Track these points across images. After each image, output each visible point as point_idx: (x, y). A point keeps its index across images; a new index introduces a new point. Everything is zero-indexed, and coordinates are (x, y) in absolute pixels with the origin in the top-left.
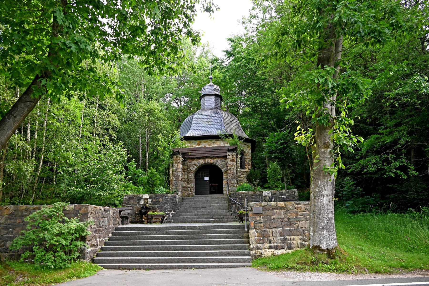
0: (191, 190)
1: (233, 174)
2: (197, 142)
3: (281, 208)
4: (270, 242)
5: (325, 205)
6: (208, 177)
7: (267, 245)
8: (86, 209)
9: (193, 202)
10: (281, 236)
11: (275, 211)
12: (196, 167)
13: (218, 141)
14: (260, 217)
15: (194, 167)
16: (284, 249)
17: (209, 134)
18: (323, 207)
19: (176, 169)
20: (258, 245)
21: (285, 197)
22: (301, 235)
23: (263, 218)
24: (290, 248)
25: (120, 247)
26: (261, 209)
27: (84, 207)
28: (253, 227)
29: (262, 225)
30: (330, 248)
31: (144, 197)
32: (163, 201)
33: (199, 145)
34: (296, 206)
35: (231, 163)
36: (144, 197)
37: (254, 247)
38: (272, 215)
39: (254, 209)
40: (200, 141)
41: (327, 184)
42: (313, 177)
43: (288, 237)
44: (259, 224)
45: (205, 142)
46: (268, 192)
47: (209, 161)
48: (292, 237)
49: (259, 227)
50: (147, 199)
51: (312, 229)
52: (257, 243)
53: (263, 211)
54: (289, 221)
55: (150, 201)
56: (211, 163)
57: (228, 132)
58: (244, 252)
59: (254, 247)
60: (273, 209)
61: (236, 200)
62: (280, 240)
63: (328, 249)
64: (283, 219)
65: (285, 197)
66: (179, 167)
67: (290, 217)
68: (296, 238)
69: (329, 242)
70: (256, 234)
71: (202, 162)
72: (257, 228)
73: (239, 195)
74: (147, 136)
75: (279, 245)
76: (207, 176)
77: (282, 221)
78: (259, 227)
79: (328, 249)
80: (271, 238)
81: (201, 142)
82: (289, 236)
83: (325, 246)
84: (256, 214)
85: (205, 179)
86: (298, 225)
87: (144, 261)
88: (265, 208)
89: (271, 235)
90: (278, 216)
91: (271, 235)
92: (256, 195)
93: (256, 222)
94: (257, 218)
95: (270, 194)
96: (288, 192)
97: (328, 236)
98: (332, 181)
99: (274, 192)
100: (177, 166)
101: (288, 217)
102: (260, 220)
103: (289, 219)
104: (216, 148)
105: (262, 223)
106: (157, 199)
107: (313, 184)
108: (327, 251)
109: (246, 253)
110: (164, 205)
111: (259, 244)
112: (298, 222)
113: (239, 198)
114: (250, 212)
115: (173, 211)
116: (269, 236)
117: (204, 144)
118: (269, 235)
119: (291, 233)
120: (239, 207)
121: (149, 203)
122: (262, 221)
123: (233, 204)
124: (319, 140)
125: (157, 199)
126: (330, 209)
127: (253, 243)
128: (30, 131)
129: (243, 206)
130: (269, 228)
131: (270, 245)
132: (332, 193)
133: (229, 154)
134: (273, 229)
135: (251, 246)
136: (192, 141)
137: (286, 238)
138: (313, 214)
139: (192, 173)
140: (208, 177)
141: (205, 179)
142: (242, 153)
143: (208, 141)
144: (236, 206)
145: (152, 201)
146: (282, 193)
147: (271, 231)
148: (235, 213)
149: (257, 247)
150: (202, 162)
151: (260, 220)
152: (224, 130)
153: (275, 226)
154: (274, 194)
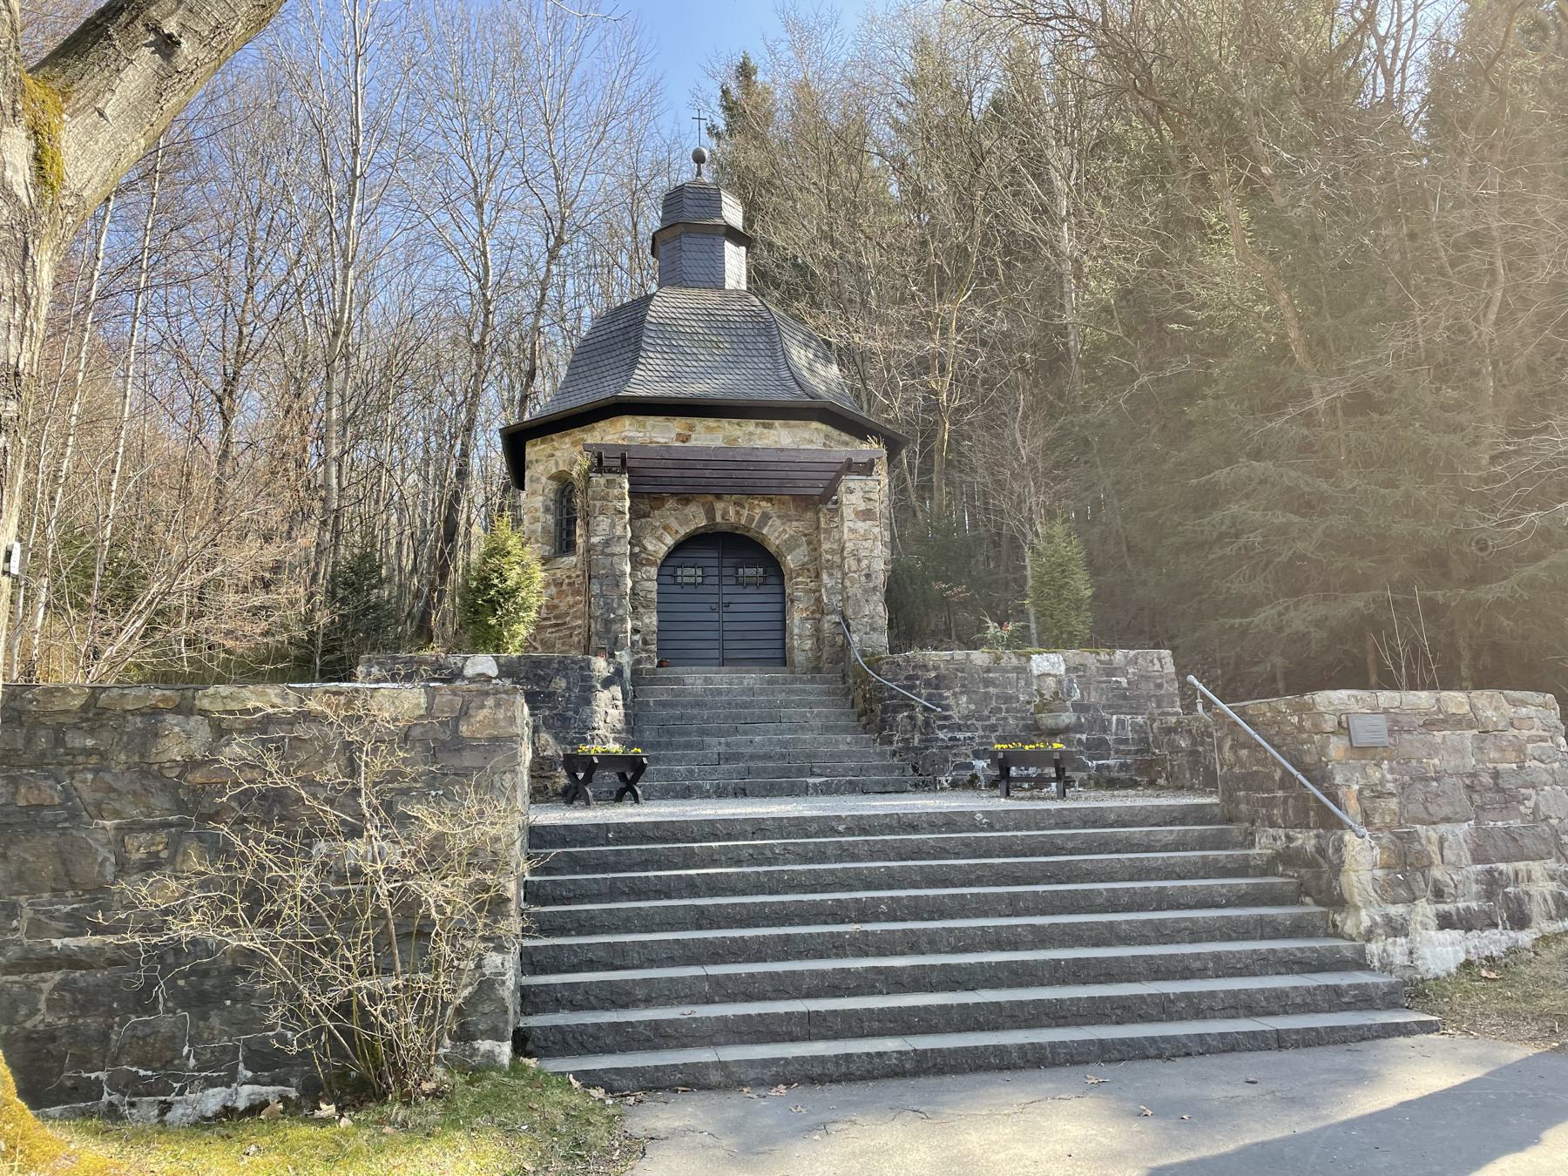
0: (645, 642)
1: (868, 576)
3: (1458, 722)
4: (1439, 894)
8: (501, 715)
10: (1476, 861)
11: (1438, 736)
12: (670, 541)
14: (1378, 765)
15: (660, 539)
16: (1496, 926)
19: (607, 543)
21: (1124, 681)
23: (1392, 771)
24: (1520, 920)
25: (643, 944)
26: (1381, 722)
27: (490, 702)
31: (469, 671)
32: (568, 689)
34: (1510, 711)
35: (861, 526)
36: (469, 671)
37: (1375, 924)
38: (1430, 756)
39: (1356, 724)
40: (690, 420)
43: (1502, 866)
44: (1382, 803)
46: (1053, 657)
48: (1521, 865)
53: (1391, 732)
54: (1499, 790)
58: (1337, 950)
59: (1375, 924)
60: (1430, 725)
61: (910, 688)
65: (1124, 681)
66: (619, 531)
67: (1500, 766)
68: (1537, 868)
70: (1377, 851)
72: (1377, 820)
73: (925, 667)
74: (43, 493)
75: (1474, 905)
80: (1437, 873)
82: (1506, 860)
87: (640, 993)
88: (1396, 722)
89: (1437, 859)
90: (1452, 763)
91: (1437, 859)
92: (1005, 671)
95: (1063, 668)
96: (1134, 661)
99: (1078, 660)
100: (613, 525)
105: (1391, 794)
106: (544, 679)
109: (1348, 954)
110: (577, 712)
111: (1394, 903)
113: (928, 684)
114: (1333, 739)
116: (1431, 864)
117: (709, 436)
118: (1430, 857)
120: (927, 723)
122: (1390, 786)
123: (896, 710)
125: (544, 679)
129: (946, 718)
130: (1423, 822)
133: (851, 484)
134: (1443, 828)
139: (651, 563)
143: (725, 422)
144: (911, 718)
146: (1110, 662)
147: (1434, 836)
148: (908, 749)
149: (1389, 920)
151: (1382, 782)
152: (792, 384)
153: (1447, 810)
154: (1076, 669)
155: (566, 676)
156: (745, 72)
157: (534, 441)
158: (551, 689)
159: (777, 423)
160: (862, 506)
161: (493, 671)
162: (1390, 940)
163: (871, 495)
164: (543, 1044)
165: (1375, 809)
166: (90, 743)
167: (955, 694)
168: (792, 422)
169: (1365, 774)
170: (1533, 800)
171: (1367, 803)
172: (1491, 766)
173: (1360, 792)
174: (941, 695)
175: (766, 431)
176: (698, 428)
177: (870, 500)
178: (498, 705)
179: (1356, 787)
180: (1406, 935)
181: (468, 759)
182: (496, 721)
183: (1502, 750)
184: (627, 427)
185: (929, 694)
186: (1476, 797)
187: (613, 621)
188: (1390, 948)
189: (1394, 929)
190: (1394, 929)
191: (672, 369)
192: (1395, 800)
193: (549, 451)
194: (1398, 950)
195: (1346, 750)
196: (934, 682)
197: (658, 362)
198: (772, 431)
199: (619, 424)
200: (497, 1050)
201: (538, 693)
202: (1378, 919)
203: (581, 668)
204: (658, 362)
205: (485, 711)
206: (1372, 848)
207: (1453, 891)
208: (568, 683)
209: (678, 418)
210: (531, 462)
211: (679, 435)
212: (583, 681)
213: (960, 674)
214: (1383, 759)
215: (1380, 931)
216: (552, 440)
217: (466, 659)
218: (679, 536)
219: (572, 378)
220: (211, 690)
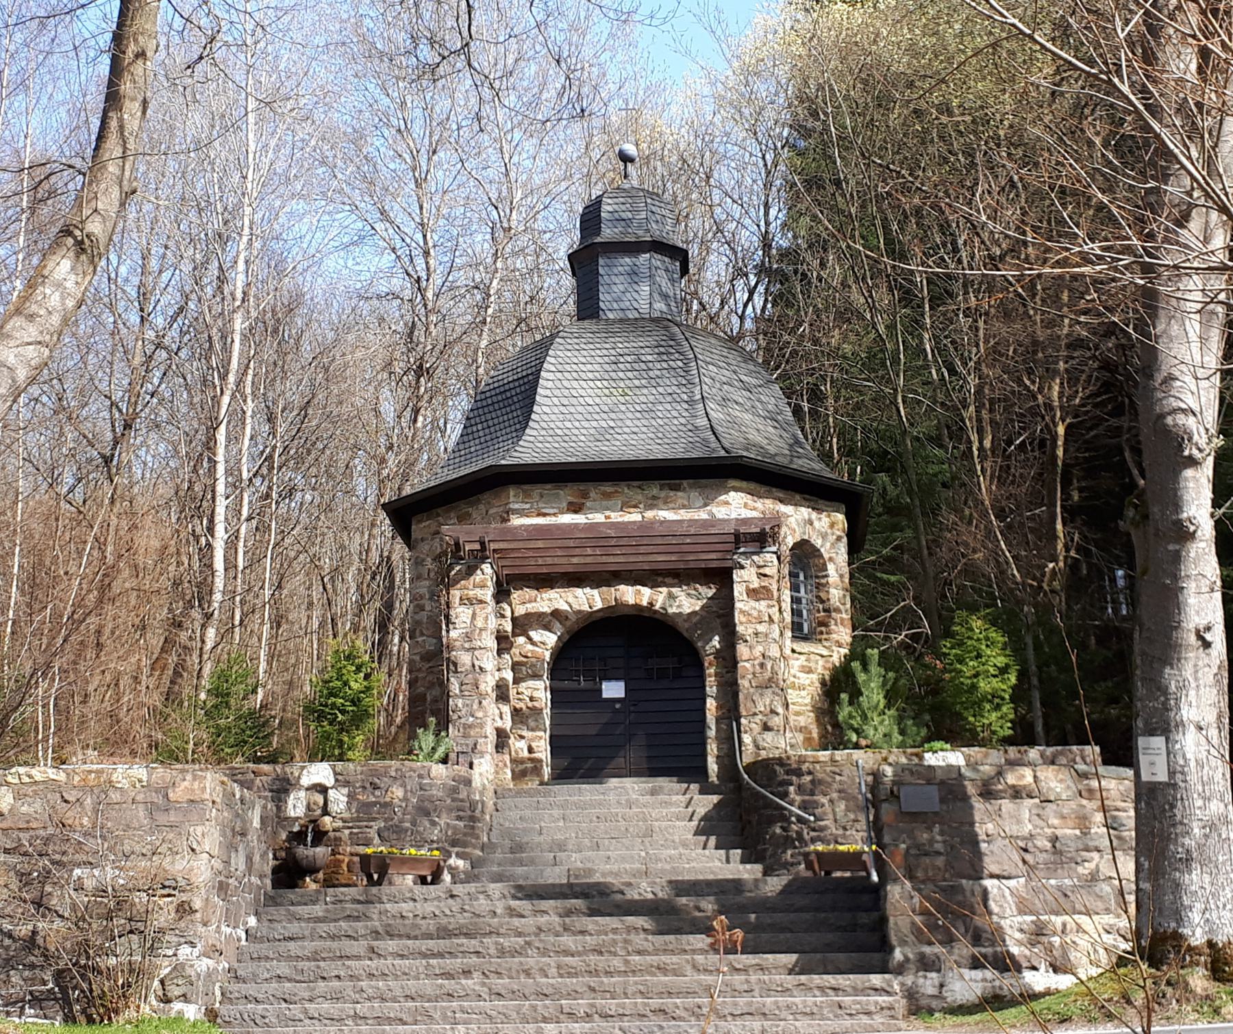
2: (567, 494)
5: (1193, 764)
6: (621, 684)
7: (964, 949)
10: (1021, 912)
13: (677, 488)
14: (930, 829)
18: (1183, 773)
19: (468, 637)
20: (927, 950)
22: (1108, 911)
23: (942, 833)
26: (934, 791)
29: (940, 861)
30: (1220, 940)
32: (405, 799)
36: (306, 781)
37: (907, 960)
41: (1196, 679)
42: (1143, 654)
44: (927, 860)
47: (632, 595)
49: (926, 871)
50: (322, 789)
51: (1146, 864)
52: (921, 942)
53: (943, 800)
55: (339, 800)
59: (907, 960)
62: (1021, 930)
63: (1211, 944)
66: (479, 623)
67: (1059, 832)
72: (920, 874)
76: (617, 679)
77: (1026, 850)
78: (926, 871)
79: (1211, 944)
81: (585, 495)
84: (914, 816)
85: (606, 694)
86: (1092, 865)
93: (913, 852)
94: (917, 833)
102: (932, 841)
105: (938, 853)
107: (1143, 679)
112: (1095, 855)
113: (800, 789)
115: (458, 855)
119: (1063, 903)
121: (333, 808)
122: (939, 847)
124: (1156, 510)
126: (1211, 780)
127: (903, 943)
128: (1062, 506)
132: (1219, 717)
135: (898, 955)
136: (537, 490)
138: (1147, 804)
140: (621, 684)
141: (606, 694)
145: (351, 797)
155: (404, 785)
157: (419, 517)
158: (388, 799)
159: (685, 483)
160: (755, 583)
161: (329, 781)
163: (767, 571)
164: (227, 1019)
167: (831, 801)
168: (703, 481)
169: (911, 835)
170: (1095, 863)
172: (1049, 831)
174: (817, 805)
175: (672, 493)
176: (592, 494)
177: (765, 575)
179: (903, 846)
180: (939, 971)
182: (193, 790)
184: (512, 499)
185: (803, 801)
186: (1028, 857)
189: (925, 964)
190: (925, 964)
191: (569, 425)
192: (942, 858)
193: (433, 528)
194: (928, 982)
198: (680, 494)
199: (503, 495)
200: (185, 1009)
201: (375, 804)
202: (911, 956)
205: (186, 783)
207: (990, 936)
208: (406, 792)
209: (570, 484)
210: (416, 540)
211: (570, 503)
213: (838, 778)
215: (911, 966)
216: (438, 515)
217: (303, 768)
218: (568, 623)
220: (13, 770)
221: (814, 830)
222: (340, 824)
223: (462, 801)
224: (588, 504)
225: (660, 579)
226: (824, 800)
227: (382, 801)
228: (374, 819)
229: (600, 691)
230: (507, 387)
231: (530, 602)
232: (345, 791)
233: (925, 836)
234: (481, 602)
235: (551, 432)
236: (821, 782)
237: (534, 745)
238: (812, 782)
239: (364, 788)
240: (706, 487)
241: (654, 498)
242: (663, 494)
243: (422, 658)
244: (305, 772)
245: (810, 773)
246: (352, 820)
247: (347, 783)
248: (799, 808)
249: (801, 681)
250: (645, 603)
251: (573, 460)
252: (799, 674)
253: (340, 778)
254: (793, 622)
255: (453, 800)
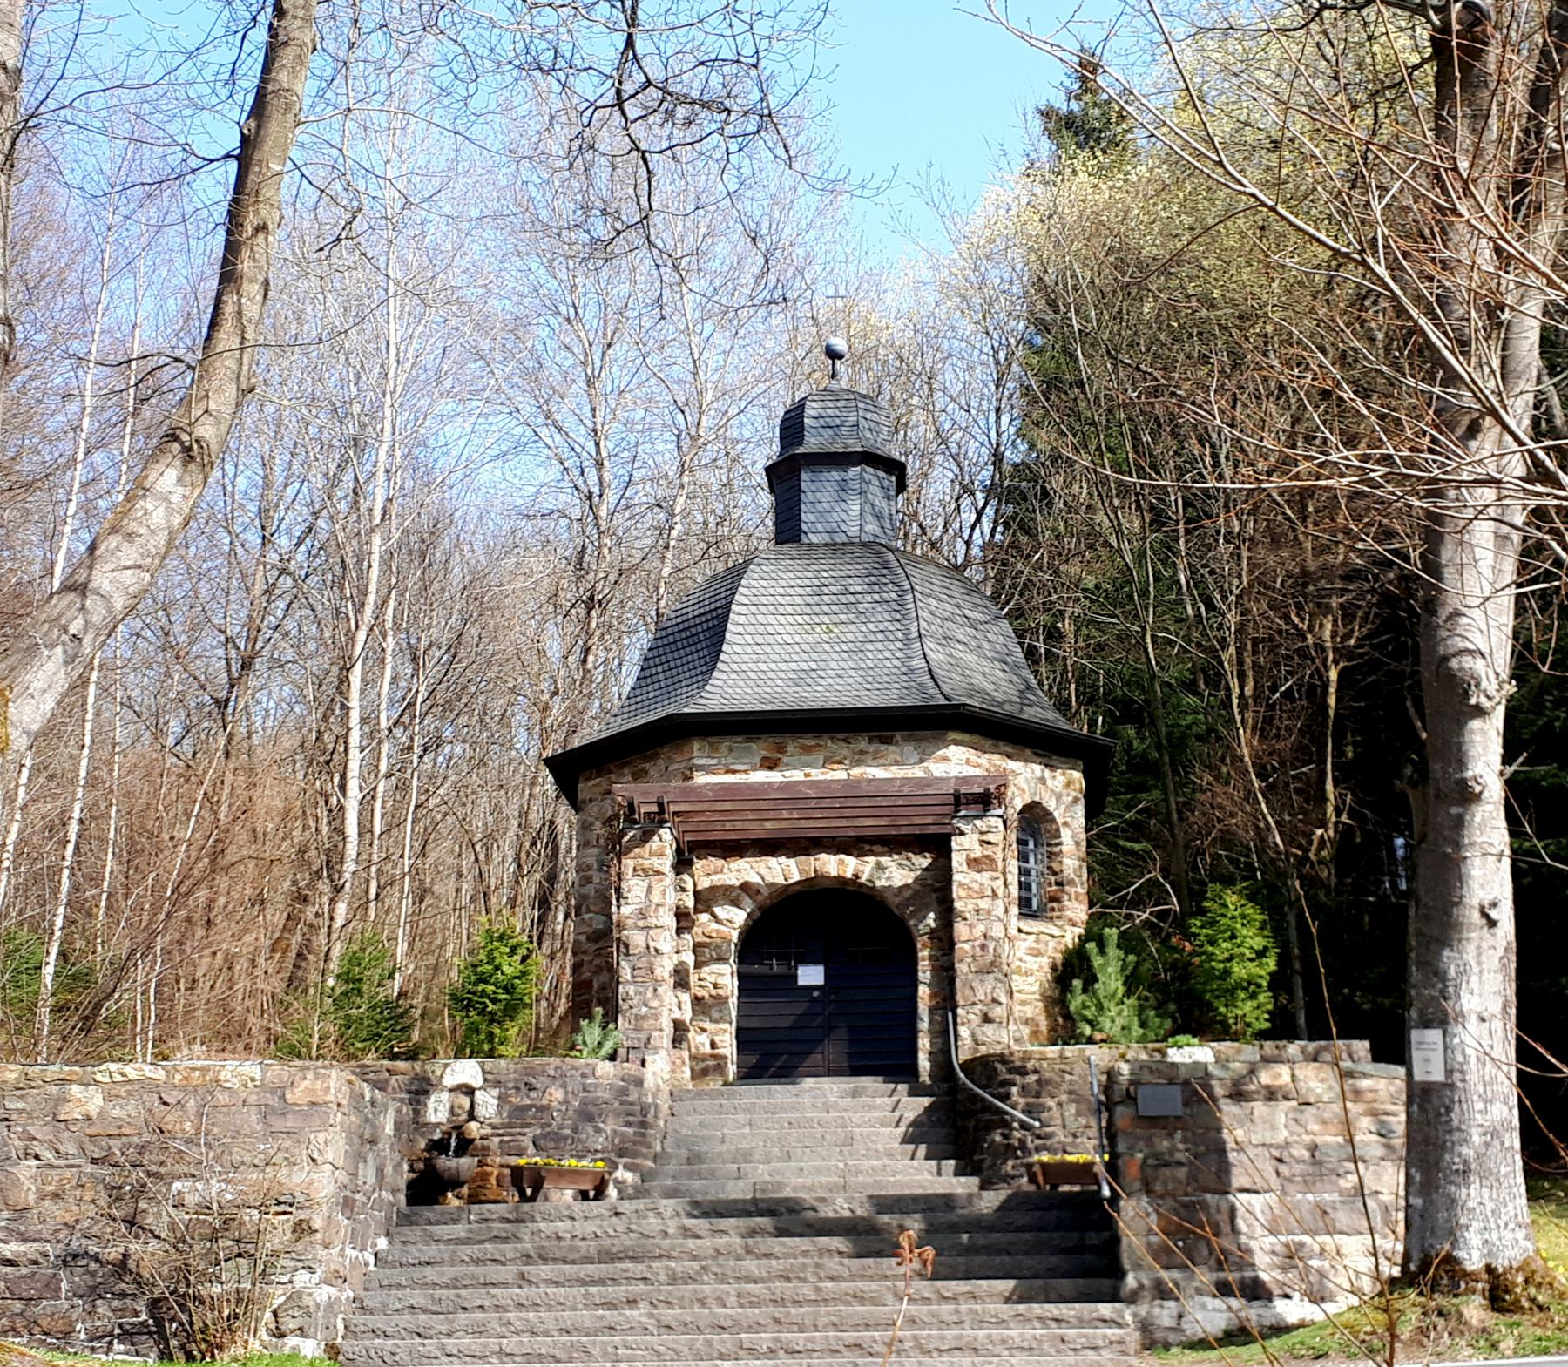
2: (760, 749)
9: (741, 1118)
13: (887, 741)
14: (1170, 1135)
17: (834, 701)
19: (642, 914)
23: (1184, 1140)
28: (1137, 1185)
29: (1182, 1173)
30: (1500, 1264)
32: (566, 1102)
33: (770, 764)
37: (1141, 1287)
41: (1479, 963)
42: (1419, 934)
44: (1167, 1172)
45: (807, 750)
47: (834, 865)
49: (1165, 1183)
53: (1186, 1103)
55: (487, 1103)
56: (841, 880)
57: (946, 689)
59: (1141, 1287)
63: (1490, 1269)
64: (1287, 1145)
66: (656, 897)
67: (1319, 1140)
69: (1495, 1235)
71: (781, 871)
72: (1158, 1188)
76: (815, 962)
77: (1280, 1160)
78: (1165, 1183)
81: (781, 749)
83: (1476, 1254)
84: (1153, 1121)
93: (1150, 1161)
97: (1490, 1206)
98: (1501, 952)
101: (1307, 1138)
103: (1314, 1148)
104: (895, 790)
105: (1180, 1164)
108: (1486, 1277)
113: (1024, 1090)
115: (627, 1167)
121: (480, 1112)
122: (1179, 1156)
127: (1137, 1267)
131: (1221, 1275)
132: (1505, 1007)
135: (1131, 1281)
136: (725, 744)
137: (1302, 1245)
142: (1035, 821)
150: (781, 871)
155: (564, 1086)
156: (1087, 69)
157: (587, 774)
158: (545, 1102)
159: (898, 736)
160: (977, 852)
161: (476, 1080)
162: (1157, 1302)
163: (990, 837)
165: (1156, 1178)
166: (20, 1106)
167: (1060, 1104)
171: (1149, 1171)
173: (1145, 1160)
175: (883, 747)
176: (790, 749)
177: (989, 843)
178: (316, 1078)
179: (1140, 1156)
181: (291, 1122)
183: (1324, 1122)
184: (696, 753)
185: (1028, 1104)
187: (644, 1018)
188: (1157, 1311)
191: (764, 667)
193: (605, 787)
194: (1165, 1312)
195: (1133, 1119)
196: (1035, 1087)
197: (746, 658)
198: (891, 748)
201: (530, 1107)
202: (1146, 1282)
203: (584, 1076)
204: (746, 658)
206: (1148, 1215)
208: (566, 1093)
212: (585, 1090)
213: (1068, 1077)
214: (1176, 1129)
217: (446, 1066)
218: (760, 898)
219: (643, 682)
220: (104, 1067)
221: (1039, 1137)
222: (488, 1130)
223: (631, 1104)
224: (785, 759)
225: (867, 847)
226: (1051, 1103)
227: (538, 1103)
228: (528, 1125)
229: (796, 976)
230: (692, 623)
231: (716, 873)
232: (496, 1092)
233: (1165, 1143)
234: (658, 873)
235: (743, 675)
236: (1048, 1082)
237: (717, 1039)
238: (1039, 1082)
239: (517, 1089)
240: (922, 739)
241: (862, 752)
242: (872, 748)
243: (588, 939)
244: (448, 1070)
245: (1036, 1071)
246: (504, 1126)
247: (497, 1084)
248: (1023, 1112)
249: (1028, 966)
250: (849, 875)
251: (768, 708)
252: (1026, 958)
253: (489, 1077)
254: (1020, 898)
255: (622, 1103)
